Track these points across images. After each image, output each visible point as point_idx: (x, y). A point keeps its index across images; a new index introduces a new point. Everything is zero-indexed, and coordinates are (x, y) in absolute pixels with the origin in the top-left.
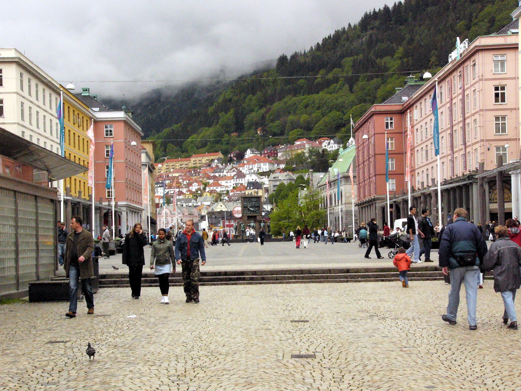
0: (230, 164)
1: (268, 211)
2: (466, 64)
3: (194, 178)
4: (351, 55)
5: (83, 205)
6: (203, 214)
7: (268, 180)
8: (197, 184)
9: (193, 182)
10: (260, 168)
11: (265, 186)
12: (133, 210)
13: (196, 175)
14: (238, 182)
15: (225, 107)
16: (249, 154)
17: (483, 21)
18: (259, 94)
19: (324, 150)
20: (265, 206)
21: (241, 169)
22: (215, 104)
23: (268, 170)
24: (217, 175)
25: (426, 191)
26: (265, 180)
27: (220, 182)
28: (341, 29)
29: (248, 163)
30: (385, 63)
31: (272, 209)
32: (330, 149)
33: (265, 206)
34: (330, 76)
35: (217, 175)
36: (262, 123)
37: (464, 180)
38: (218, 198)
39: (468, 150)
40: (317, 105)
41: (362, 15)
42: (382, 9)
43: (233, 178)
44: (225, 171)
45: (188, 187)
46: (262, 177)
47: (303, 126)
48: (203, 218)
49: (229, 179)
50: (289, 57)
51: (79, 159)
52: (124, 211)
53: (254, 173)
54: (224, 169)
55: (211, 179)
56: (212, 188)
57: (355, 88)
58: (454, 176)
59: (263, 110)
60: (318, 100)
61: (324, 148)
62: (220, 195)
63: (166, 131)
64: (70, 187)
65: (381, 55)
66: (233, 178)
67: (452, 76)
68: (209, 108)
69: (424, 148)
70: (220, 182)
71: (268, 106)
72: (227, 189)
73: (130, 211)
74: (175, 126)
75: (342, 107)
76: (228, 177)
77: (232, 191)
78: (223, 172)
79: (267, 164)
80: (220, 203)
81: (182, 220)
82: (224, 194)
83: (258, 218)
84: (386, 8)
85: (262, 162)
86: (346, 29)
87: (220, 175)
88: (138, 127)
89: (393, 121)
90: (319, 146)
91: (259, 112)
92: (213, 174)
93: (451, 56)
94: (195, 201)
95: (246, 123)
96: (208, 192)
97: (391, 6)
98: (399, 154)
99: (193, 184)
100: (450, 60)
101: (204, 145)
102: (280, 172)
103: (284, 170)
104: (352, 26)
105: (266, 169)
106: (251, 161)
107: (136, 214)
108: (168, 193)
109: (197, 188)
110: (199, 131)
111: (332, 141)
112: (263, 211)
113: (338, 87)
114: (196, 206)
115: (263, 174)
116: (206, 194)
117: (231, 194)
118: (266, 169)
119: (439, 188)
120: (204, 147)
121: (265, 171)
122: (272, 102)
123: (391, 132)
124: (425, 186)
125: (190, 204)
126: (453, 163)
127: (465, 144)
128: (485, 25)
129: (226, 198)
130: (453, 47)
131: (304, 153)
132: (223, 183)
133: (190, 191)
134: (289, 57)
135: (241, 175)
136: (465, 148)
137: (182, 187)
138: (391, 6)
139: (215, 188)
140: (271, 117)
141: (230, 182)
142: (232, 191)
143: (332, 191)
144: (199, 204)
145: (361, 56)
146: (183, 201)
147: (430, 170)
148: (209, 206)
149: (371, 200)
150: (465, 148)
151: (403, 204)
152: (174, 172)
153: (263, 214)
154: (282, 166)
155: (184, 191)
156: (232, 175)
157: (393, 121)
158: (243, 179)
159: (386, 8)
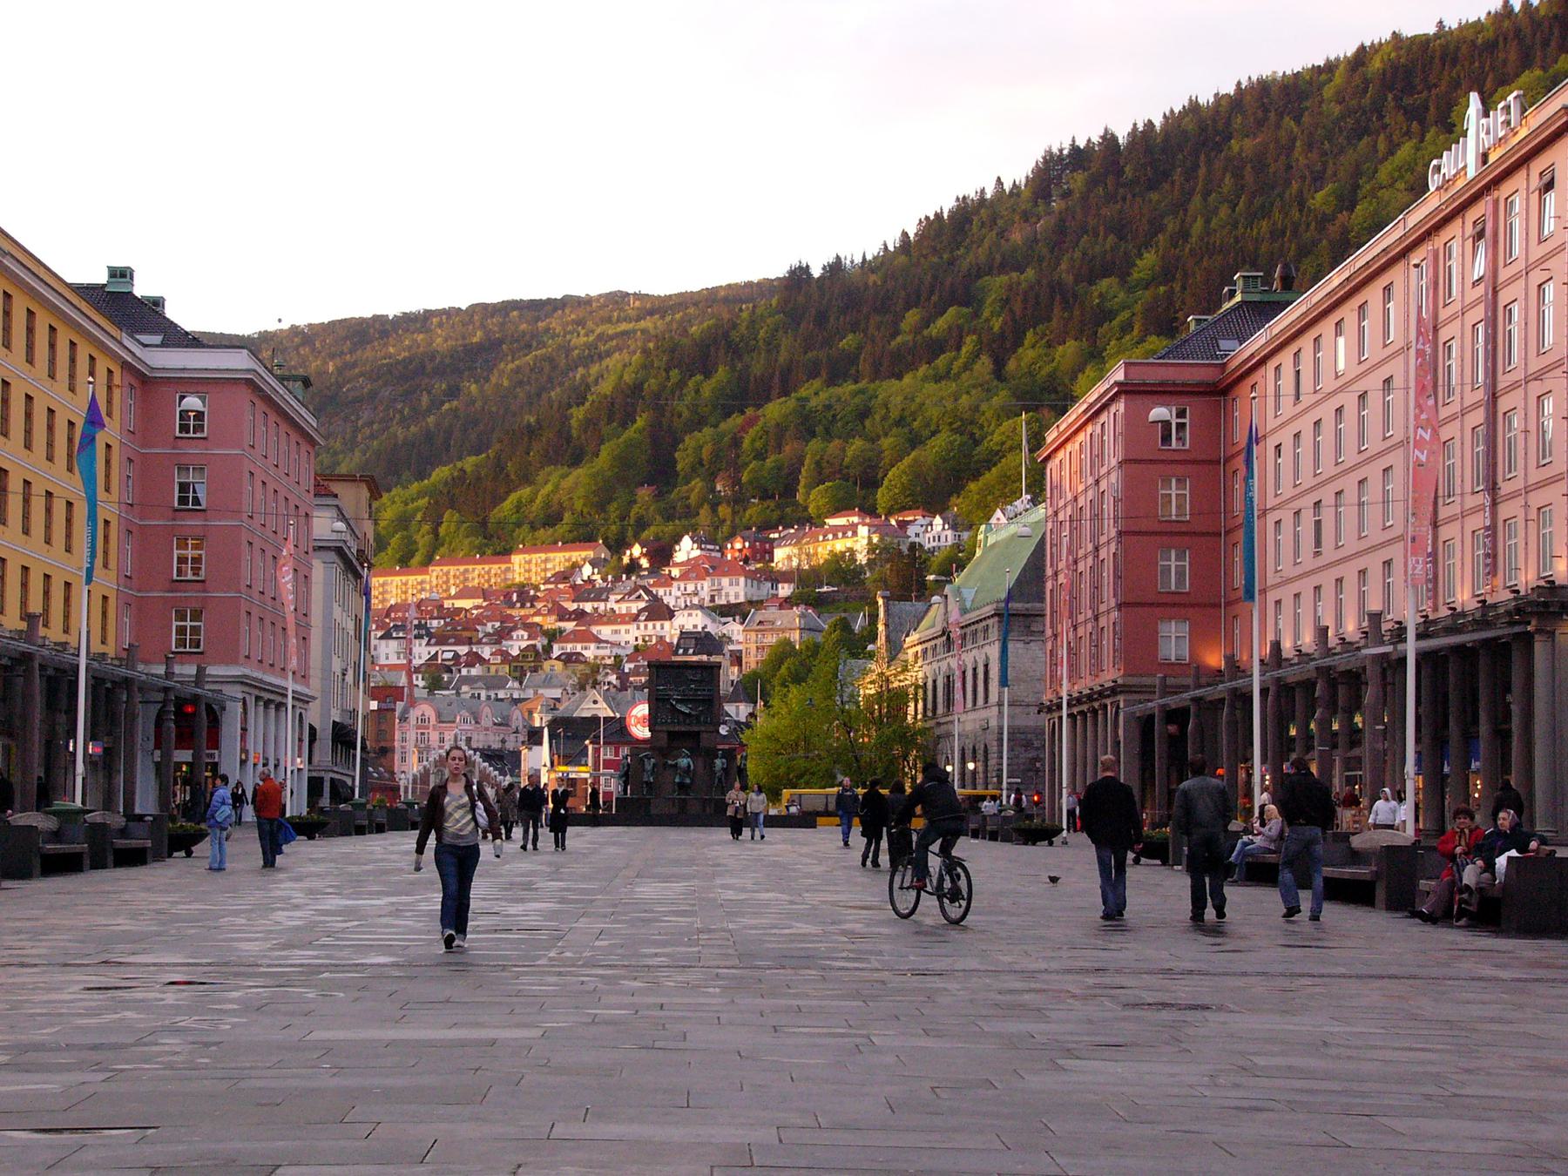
0: (628, 578)
1: (738, 723)
2: (1506, 189)
3: (517, 613)
4: (1003, 268)
5: (42, 667)
6: (537, 724)
7: (741, 628)
8: (526, 635)
9: (514, 628)
10: (719, 590)
11: (731, 647)
12: (267, 696)
13: (523, 606)
14: (650, 631)
15: (622, 407)
16: (686, 550)
17: (1391, 186)
18: (722, 373)
19: (913, 546)
20: (729, 708)
21: (661, 592)
22: (590, 398)
23: (742, 599)
24: (588, 607)
25: (1342, 662)
26: (734, 629)
27: (595, 629)
28: (972, 195)
29: (684, 577)
30: (1101, 295)
31: (752, 715)
32: (933, 544)
33: (729, 708)
34: (940, 325)
35: (588, 607)
36: (726, 459)
37: (1451, 630)
38: (590, 678)
39: (1505, 511)
40: (895, 414)
41: (1038, 155)
42: (1096, 139)
43: (635, 618)
44: (613, 598)
45: (498, 642)
46: (724, 620)
47: (852, 472)
48: (534, 737)
49: (623, 623)
50: (816, 272)
51: (27, 483)
52: (234, 699)
53: (701, 607)
54: (609, 591)
55: (569, 620)
56: (569, 647)
57: (1011, 365)
58: (1436, 609)
59: (736, 420)
60: (899, 399)
61: (913, 539)
62: (596, 669)
63: (441, 473)
64: (46, 609)
65: (1092, 275)
66: (635, 618)
67: (1438, 241)
68: (574, 410)
69: (1351, 495)
70: (595, 629)
71: (750, 412)
72: (616, 651)
73: (258, 698)
74: (472, 459)
75: (971, 423)
76: (621, 615)
77: (631, 659)
78: (606, 600)
79: (742, 580)
80: (593, 694)
81: (469, 740)
82: (605, 666)
83: (705, 739)
84: (1109, 139)
85: (724, 574)
86: (912, 236)
87: (596, 609)
88: (303, 411)
89: (1186, 421)
90: (900, 533)
91: (723, 426)
92: (574, 606)
93: (1438, 169)
94: (516, 685)
95: (683, 460)
96: (558, 658)
97: (1122, 134)
98: (1203, 534)
99: (514, 635)
100: (1434, 182)
101: (551, 519)
102: (781, 607)
103: (787, 603)
104: (1007, 187)
105: (737, 596)
106: (693, 570)
107: (272, 712)
108: (436, 656)
109: (524, 644)
110: (540, 479)
111: (938, 520)
112: (725, 723)
113: (961, 361)
114: (516, 701)
115: (727, 611)
116: (553, 666)
117: (628, 667)
118: (737, 596)
119: (1411, 648)
120: (549, 524)
121: (733, 600)
122: (764, 398)
123: (1177, 457)
124: (1333, 641)
125: (501, 695)
126: (1435, 563)
127: (1493, 488)
128: (1400, 191)
129: (613, 678)
130: (1452, 131)
131: (852, 552)
132: (605, 631)
133: (505, 656)
134: (816, 272)
135: (660, 612)
136: (1494, 504)
137: (479, 642)
138: (1122, 134)
139: (579, 648)
140: (758, 444)
141: (627, 632)
142: (631, 659)
143: (954, 663)
144: (530, 693)
145: (1030, 273)
146: (480, 684)
147: (1328, 592)
148: (558, 700)
149: (1100, 693)
150: (1494, 504)
151: (1232, 707)
152: (459, 596)
153: (723, 730)
154: (785, 590)
155: (486, 652)
156: (634, 611)
157: (1186, 421)
158: (667, 624)
159: (1109, 139)
